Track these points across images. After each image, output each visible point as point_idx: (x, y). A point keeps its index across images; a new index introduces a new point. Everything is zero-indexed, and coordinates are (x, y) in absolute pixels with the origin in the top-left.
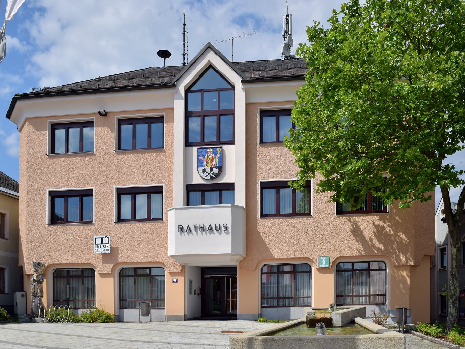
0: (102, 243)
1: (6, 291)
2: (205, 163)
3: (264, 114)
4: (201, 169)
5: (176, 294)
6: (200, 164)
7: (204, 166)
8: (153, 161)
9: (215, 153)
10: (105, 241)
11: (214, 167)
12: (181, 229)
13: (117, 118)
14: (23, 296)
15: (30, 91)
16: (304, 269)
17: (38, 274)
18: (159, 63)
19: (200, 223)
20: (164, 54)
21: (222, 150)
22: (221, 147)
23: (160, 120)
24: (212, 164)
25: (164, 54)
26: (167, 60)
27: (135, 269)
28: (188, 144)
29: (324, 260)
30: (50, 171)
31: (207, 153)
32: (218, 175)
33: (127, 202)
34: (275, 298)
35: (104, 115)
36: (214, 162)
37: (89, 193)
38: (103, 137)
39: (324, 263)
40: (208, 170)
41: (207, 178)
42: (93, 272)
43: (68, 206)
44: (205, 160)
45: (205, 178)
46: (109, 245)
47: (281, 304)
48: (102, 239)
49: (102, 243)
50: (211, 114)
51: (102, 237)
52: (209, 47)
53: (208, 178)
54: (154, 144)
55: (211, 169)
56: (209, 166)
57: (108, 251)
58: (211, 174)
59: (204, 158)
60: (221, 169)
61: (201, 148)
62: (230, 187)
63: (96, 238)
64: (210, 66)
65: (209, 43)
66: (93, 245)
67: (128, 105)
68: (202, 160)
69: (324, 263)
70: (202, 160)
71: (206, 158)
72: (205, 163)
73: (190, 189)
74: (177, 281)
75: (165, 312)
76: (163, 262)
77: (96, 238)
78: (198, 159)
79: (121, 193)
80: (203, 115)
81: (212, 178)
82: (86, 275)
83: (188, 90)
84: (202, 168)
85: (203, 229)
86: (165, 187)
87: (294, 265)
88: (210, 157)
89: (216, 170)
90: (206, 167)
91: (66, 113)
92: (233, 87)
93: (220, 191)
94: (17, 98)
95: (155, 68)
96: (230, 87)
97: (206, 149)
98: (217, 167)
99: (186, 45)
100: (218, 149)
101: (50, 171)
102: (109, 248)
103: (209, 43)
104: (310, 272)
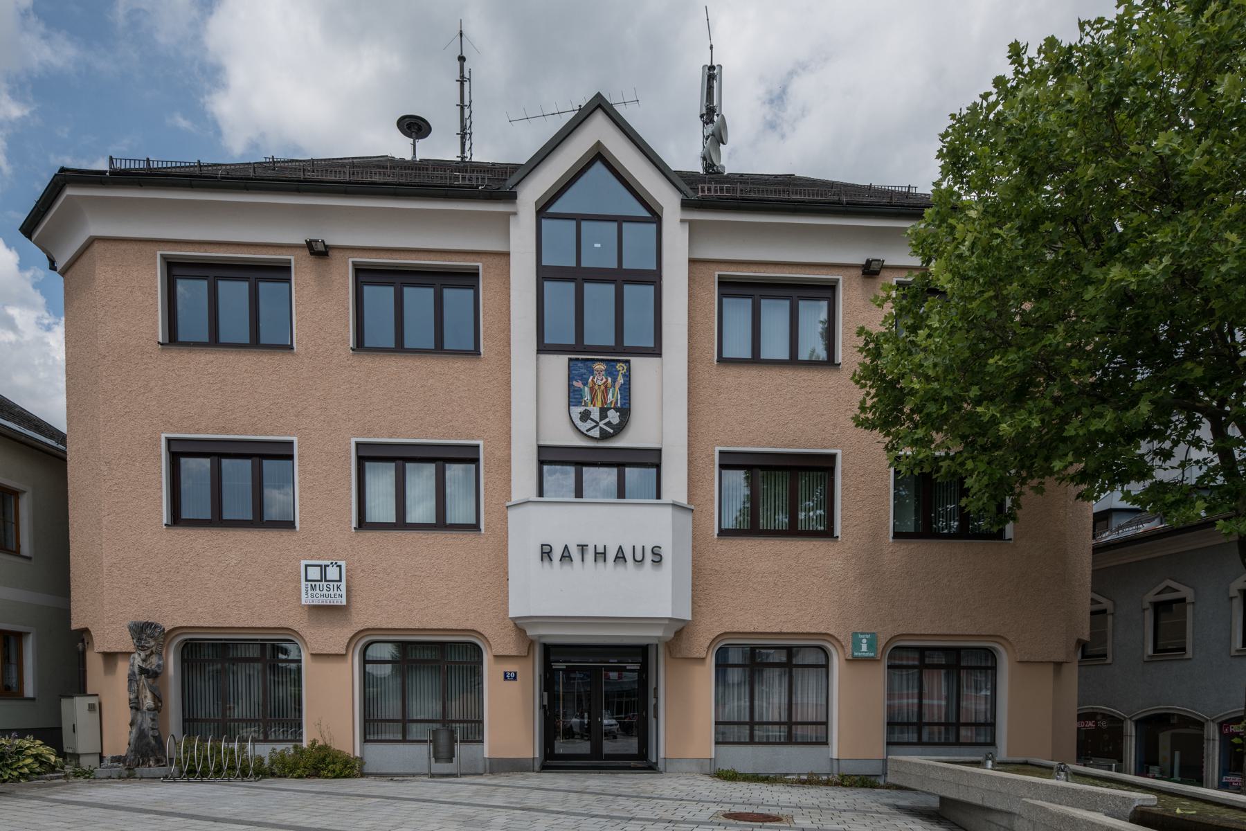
0: (324, 577)
1: (29, 691)
2: (588, 397)
3: (730, 287)
4: (577, 411)
5: (509, 711)
6: (574, 397)
7: (586, 405)
8: (452, 383)
9: (612, 373)
10: (332, 573)
11: (609, 409)
12: (546, 553)
13: (164, 257)
14: (91, 707)
15: (102, 165)
16: (810, 658)
17: (148, 652)
18: (400, 147)
19: (595, 540)
20: (414, 127)
21: (629, 370)
22: (628, 362)
23: (468, 278)
24: (604, 400)
25: (414, 127)
26: (420, 143)
27: (922, 650)
28: (543, 348)
29: (864, 641)
30: (170, 387)
31: (592, 372)
32: (620, 428)
33: (381, 482)
34: (784, 723)
35: (319, 252)
36: (610, 396)
37: (283, 452)
38: (319, 308)
39: (864, 648)
40: (595, 415)
41: (591, 433)
42: (478, 651)
43: (227, 482)
44: (587, 390)
45: (590, 433)
46: (343, 585)
47: (925, 738)
48: (323, 569)
49: (324, 577)
50: (600, 276)
51: (323, 563)
52: (599, 105)
53: (596, 433)
54: (451, 344)
55: (603, 413)
56: (599, 404)
57: (339, 599)
58: (601, 424)
59: (585, 384)
60: (625, 412)
61: (577, 360)
62: (651, 459)
63: (306, 566)
64: (599, 156)
65: (599, 95)
66: (314, 578)
67: (403, 228)
68: (580, 390)
69: (864, 648)
70: (580, 390)
71: (590, 385)
72: (588, 397)
73: (548, 456)
74: (515, 678)
75: (487, 750)
76: (480, 630)
77: (306, 566)
78: (570, 386)
79: (368, 455)
80: (579, 276)
81: (605, 436)
82: (272, 657)
83: (543, 210)
84: (581, 409)
85: (600, 555)
86: (485, 449)
87: (790, 650)
88: (600, 383)
89: (613, 416)
90: (590, 408)
91: (199, 233)
92: (655, 216)
93: (620, 466)
94: (65, 178)
95: (392, 159)
96: (646, 214)
97: (589, 364)
98: (617, 409)
99: (467, 111)
100: (619, 366)
101: (170, 387)
102: (344, 592)
103: (599, 95)
104: (826, 666)
